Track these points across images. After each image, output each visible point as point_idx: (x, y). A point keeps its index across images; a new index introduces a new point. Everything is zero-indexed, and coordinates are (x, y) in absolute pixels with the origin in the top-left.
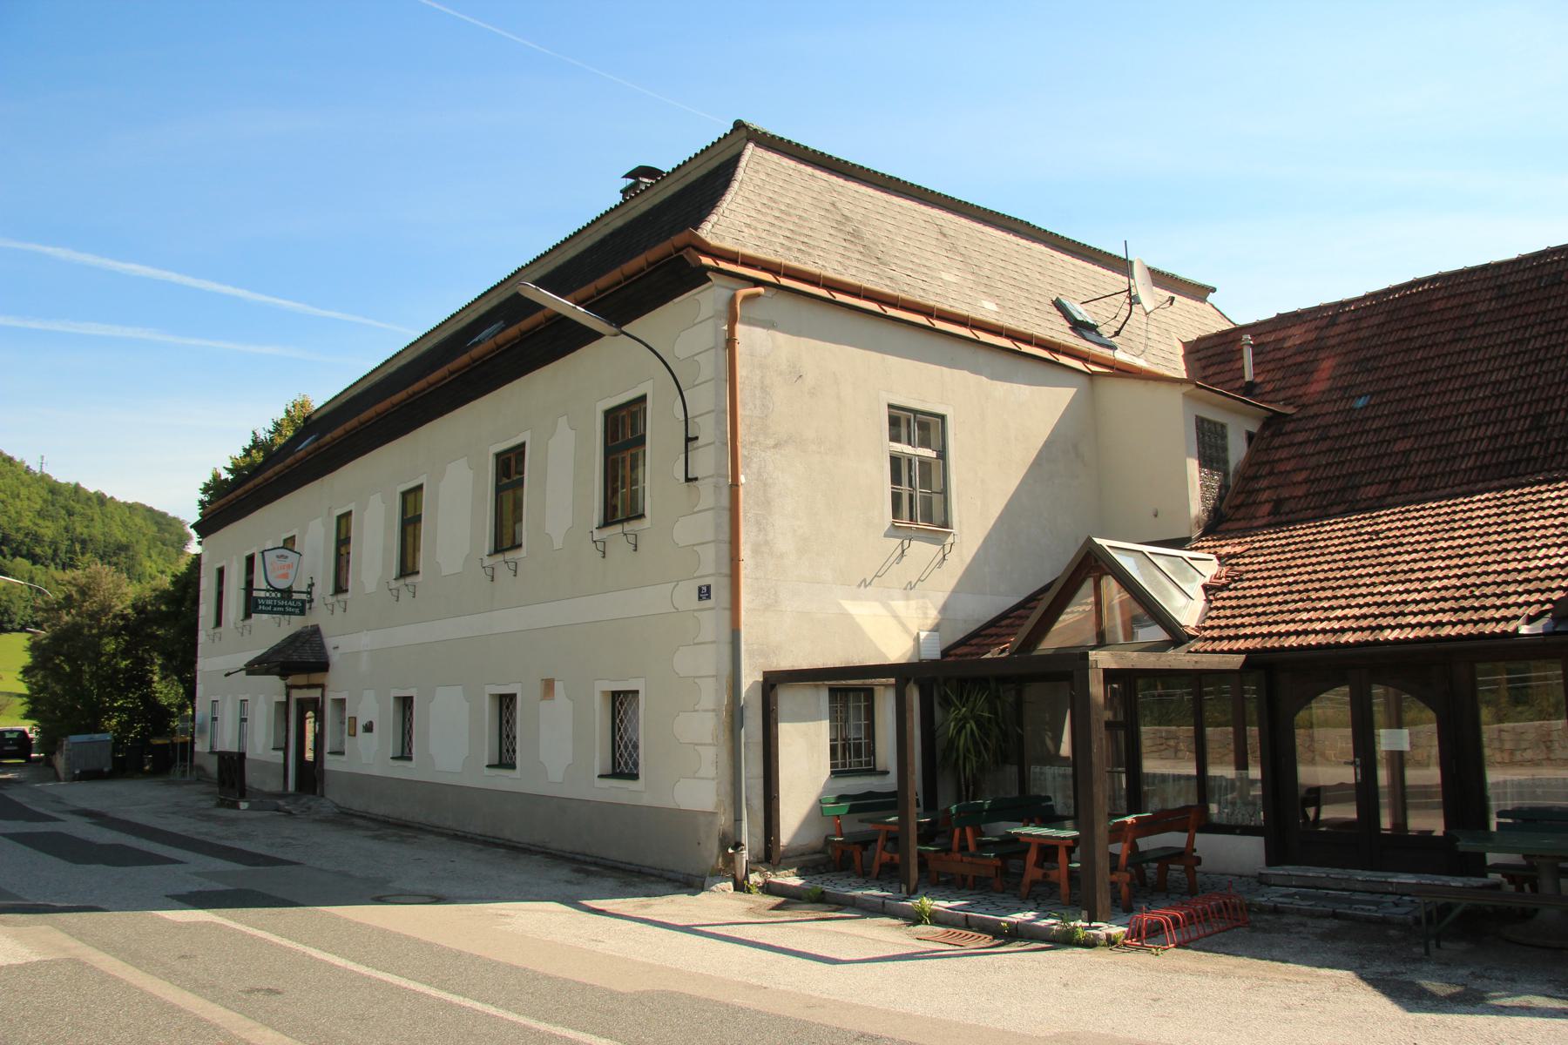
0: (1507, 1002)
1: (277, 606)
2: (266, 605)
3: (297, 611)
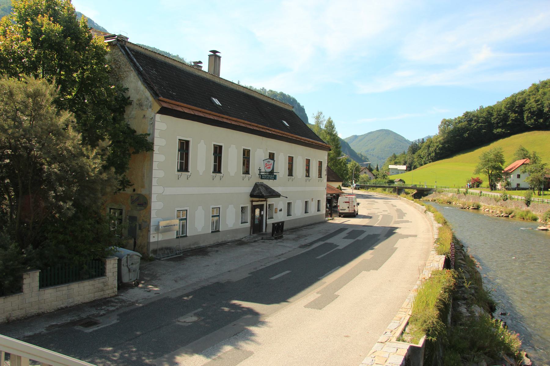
0: (190, 324)
1: (267, 177)
2: (264, 177)
3: (273, 178)
